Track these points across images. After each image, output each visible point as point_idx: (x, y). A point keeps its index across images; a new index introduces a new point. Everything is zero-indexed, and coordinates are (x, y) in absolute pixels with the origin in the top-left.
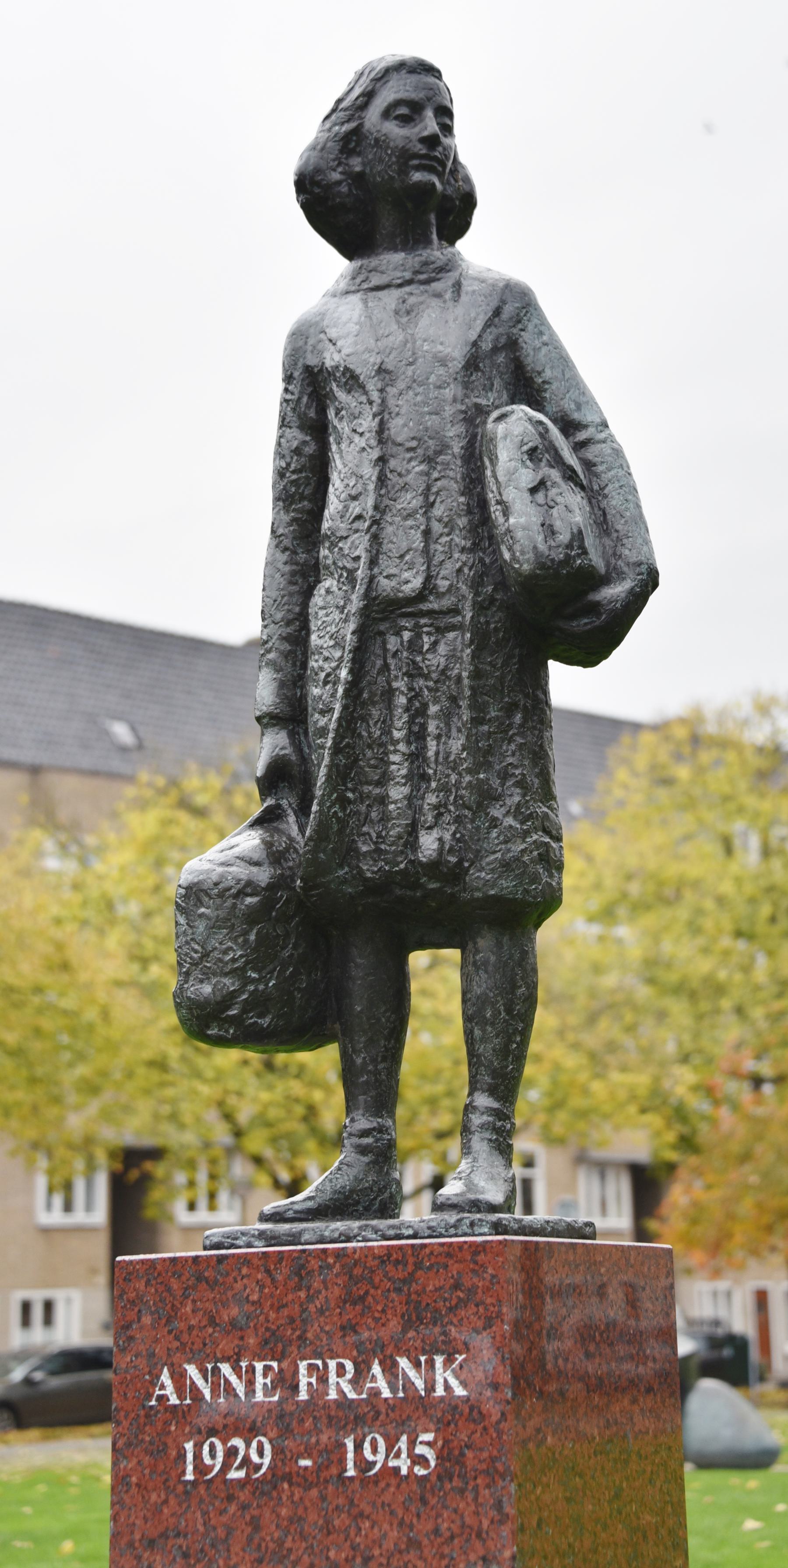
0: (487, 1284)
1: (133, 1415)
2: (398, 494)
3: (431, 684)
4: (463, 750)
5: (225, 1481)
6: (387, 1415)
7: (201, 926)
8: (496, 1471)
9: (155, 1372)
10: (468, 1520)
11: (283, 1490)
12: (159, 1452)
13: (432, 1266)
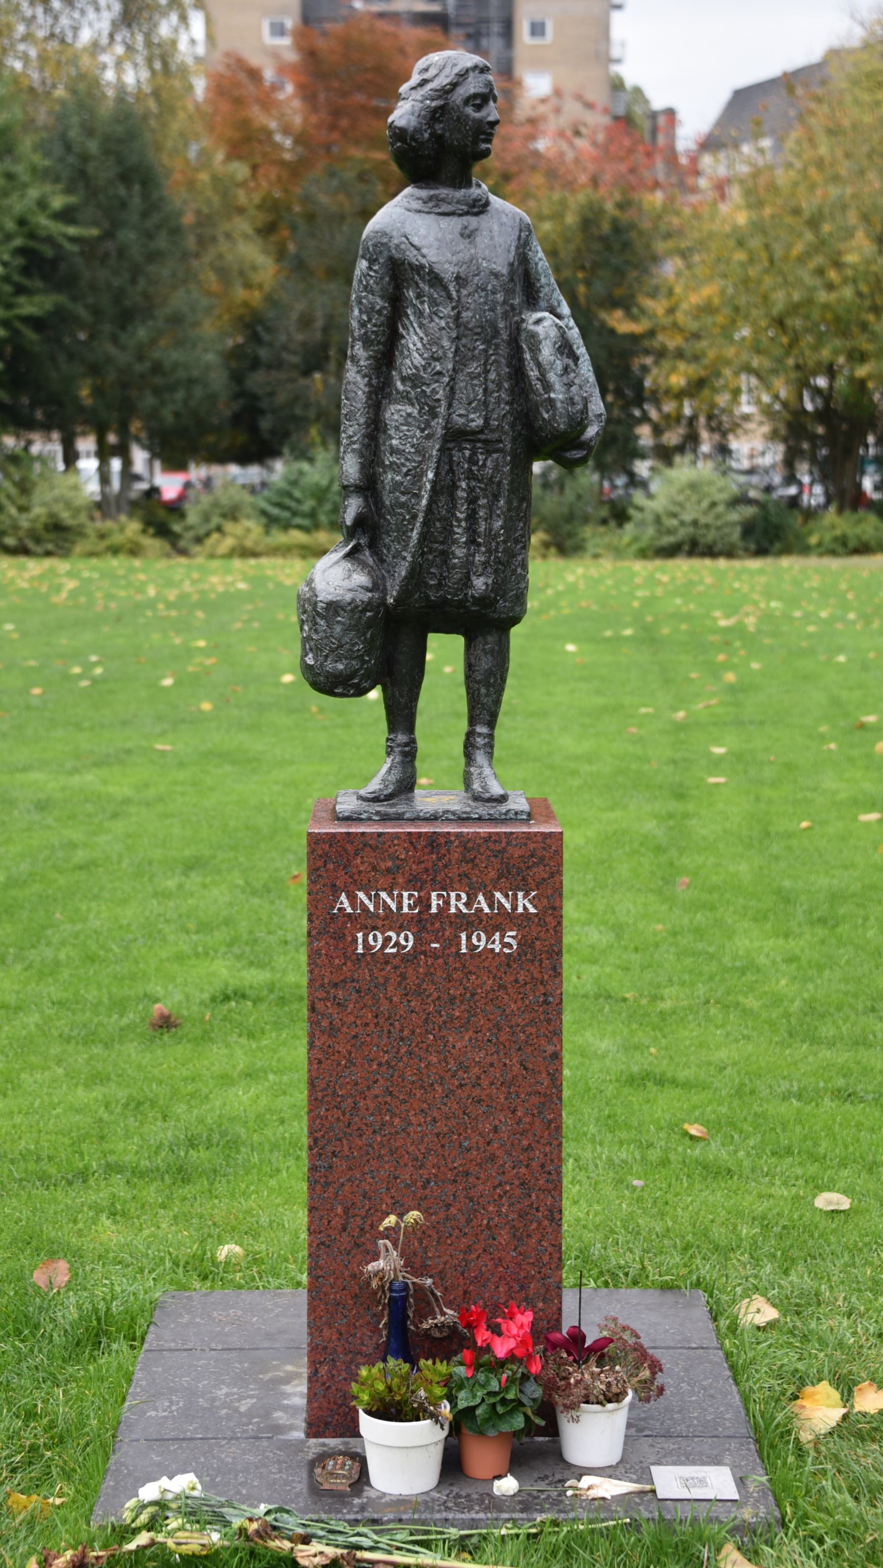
7: (338, 629)
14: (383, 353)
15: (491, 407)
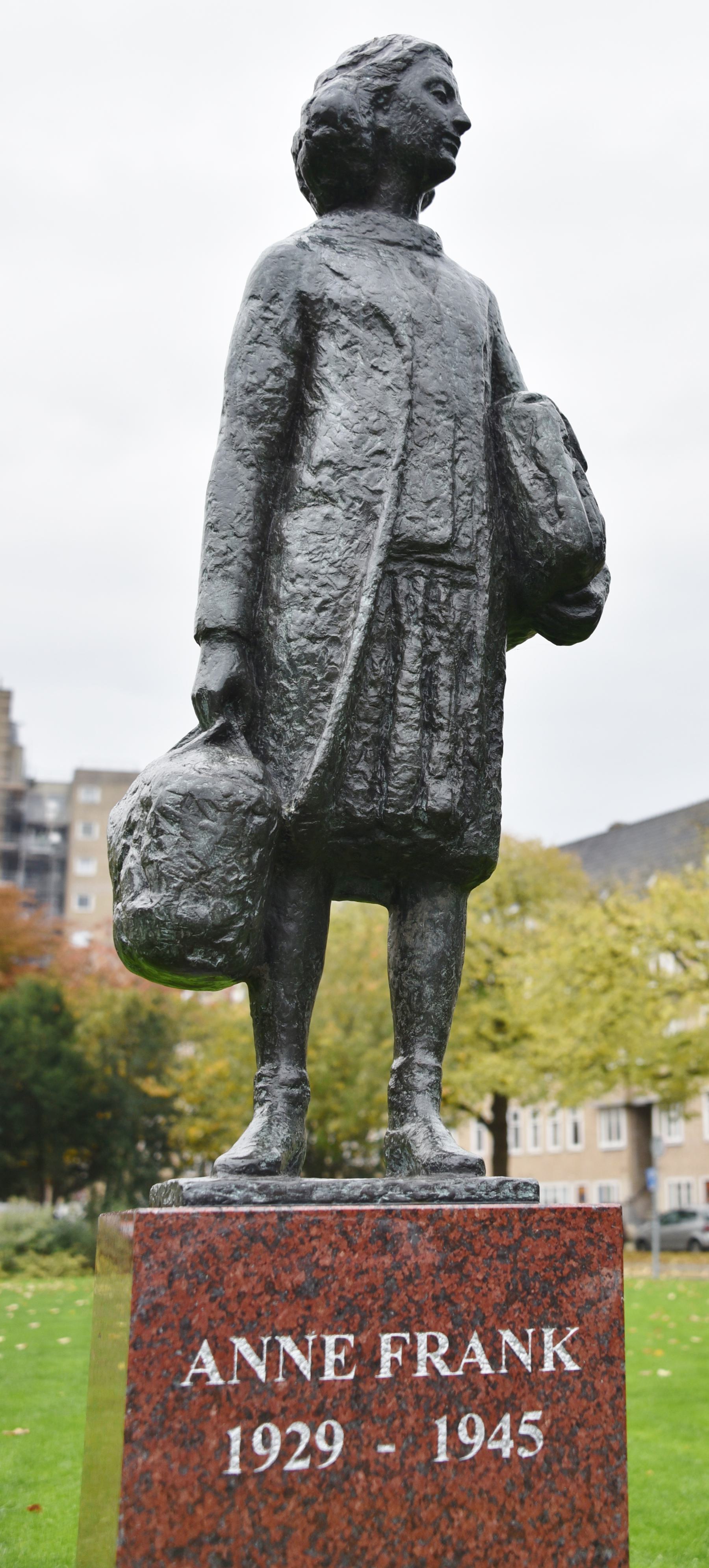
0: (603, 1253)
1: (158, 1398)
2: (426, 442)
3: (445, 634)
4: (475, 707)
5: (283, 1473)
6: (488, 1393)
7: (203, 842)
8: (611, 1449)
9: (190, 1347)
10: (578, 1503)
11: (358, 1481)
12: (193, 1442)
13: (541, 1232)
14: (279, 435)
15: (461, 514)
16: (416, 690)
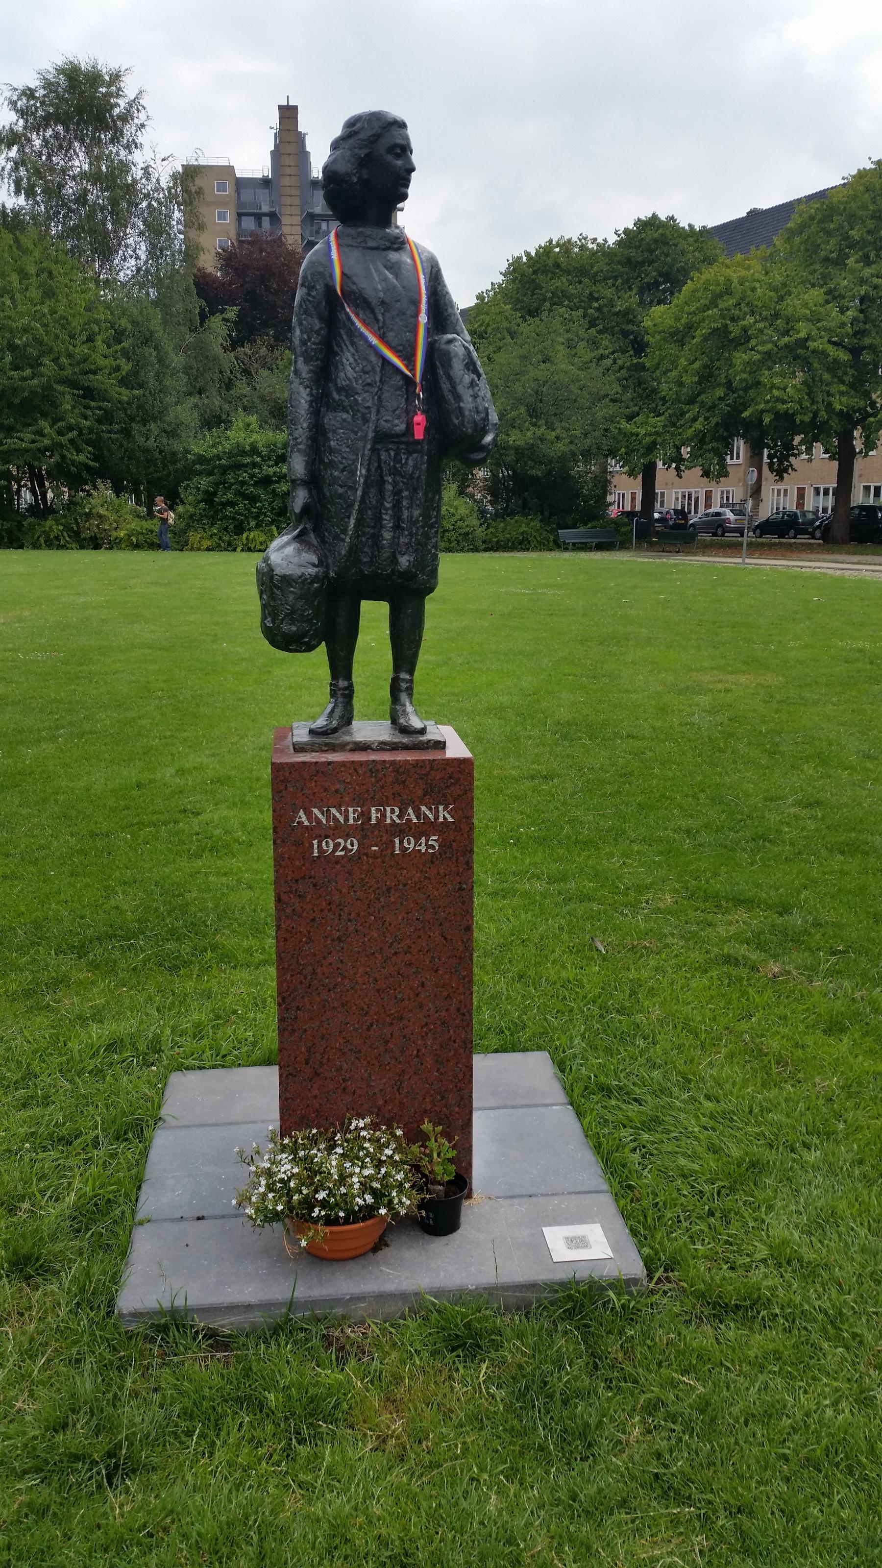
16: (390, 512)
